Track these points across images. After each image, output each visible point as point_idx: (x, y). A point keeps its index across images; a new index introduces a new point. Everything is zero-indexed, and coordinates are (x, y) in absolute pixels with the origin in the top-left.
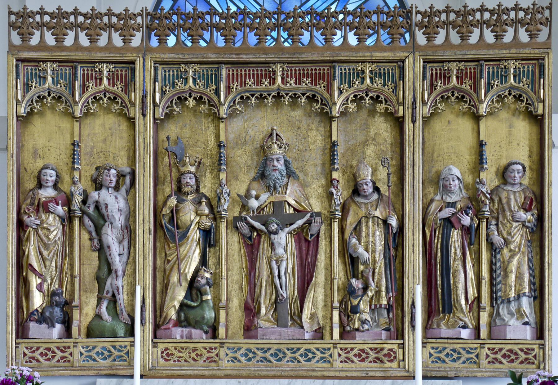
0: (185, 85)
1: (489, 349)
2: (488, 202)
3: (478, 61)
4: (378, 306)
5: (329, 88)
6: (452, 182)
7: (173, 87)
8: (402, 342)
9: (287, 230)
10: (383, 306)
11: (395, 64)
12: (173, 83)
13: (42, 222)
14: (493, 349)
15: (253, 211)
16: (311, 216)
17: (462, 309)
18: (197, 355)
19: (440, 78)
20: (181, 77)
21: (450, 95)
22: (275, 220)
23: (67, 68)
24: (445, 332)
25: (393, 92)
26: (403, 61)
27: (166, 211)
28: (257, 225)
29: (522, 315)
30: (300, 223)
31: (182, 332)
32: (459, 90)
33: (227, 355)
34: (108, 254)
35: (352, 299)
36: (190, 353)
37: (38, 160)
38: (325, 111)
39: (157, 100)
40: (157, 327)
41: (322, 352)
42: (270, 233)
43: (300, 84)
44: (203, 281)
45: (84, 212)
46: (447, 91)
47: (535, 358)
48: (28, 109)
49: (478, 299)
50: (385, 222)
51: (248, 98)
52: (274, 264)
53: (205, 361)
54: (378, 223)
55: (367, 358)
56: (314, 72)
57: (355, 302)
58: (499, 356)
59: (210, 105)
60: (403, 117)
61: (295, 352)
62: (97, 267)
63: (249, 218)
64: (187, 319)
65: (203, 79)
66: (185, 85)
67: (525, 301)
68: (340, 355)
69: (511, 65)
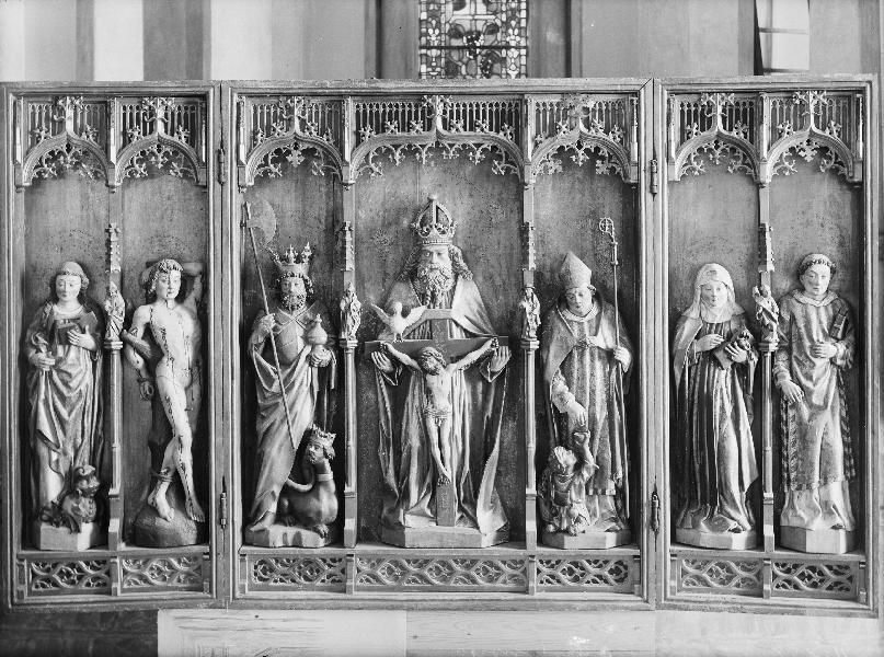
6: (716, 293)
12: (269, 126)
13: (59, 361)
17: (734, 501)
19: (696, 120)
20: (282, 119)
22: (433, 350)
23: (99, 106)
24: (706, 534)
25: (621, 142)
28: (405, 358)
29: (831, 513)
30: (474, 356)
31: (285, 534)
32: (729, 140)
34: (167, 410)
38: (512, 172)
39: (243, 158)
43: (471, 129)
45: (126, 342)
48: (34, 174)
59: (329, 163)
60: (637, 185)
62: (150, 426)
65: (397, 119)
69: (811, 98)
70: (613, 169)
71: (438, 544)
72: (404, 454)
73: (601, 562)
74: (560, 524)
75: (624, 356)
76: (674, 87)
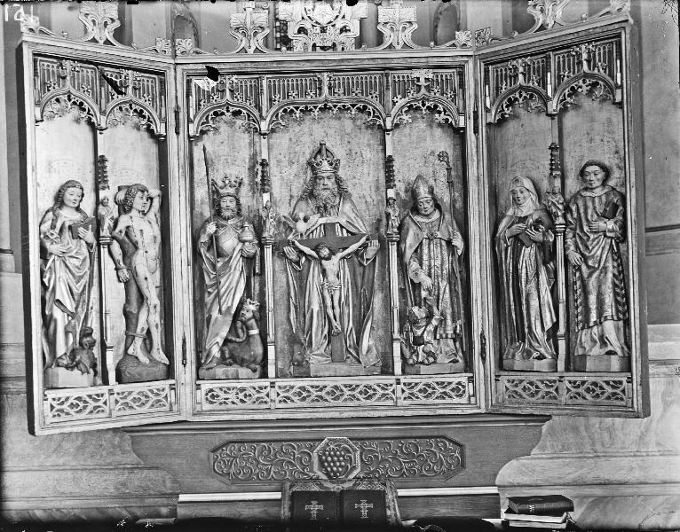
0: (222, 98)
1: (570, 382)
2: (560, 214)
3: (544, 52)
4: (444, 336)
5: (382, 97)
6: (519, 195)
7: (209, 102)
8: (471, 375)
9: (340, 255)
10: (449, 336)
11: (454, 70)
14: (575, 382)
15: (302, 235)
16: (367, 239)
18: (245, 396)
21: (517, 96)
25: (452, 101)
26: (462, 67)
27: (204, 238)
28: (307, 250)
30: (354, 247)
33: (278, 394)
35: (414, 329)
36: (237, 394)
37: (54, 175)
39: (192, 117)
40: (199, 366)
41: (383, 389)
42: (321, 258)
44: (249, 315)
46: (513, 92)
47: (624, 394)
49: (556, 326)
50: (449, 243)
51: (292, 111)
52: (326, 293)
53: (254, 402)
54: (441, 245)
55: (434, 393)
56: (364, 81)
57: (419, 333)
58: (581, 390)
61: (354, 389)
63: (297, 243)
64: (232, 356)
66: (222, 98)
67: (609, 326)
68: (403, 391)
70: (447, 120)
71: (333, 374)
72: (308, 316)
73: (354, 386)
74: (418, 358)
75: (458, 242)
76: (489, 59)
